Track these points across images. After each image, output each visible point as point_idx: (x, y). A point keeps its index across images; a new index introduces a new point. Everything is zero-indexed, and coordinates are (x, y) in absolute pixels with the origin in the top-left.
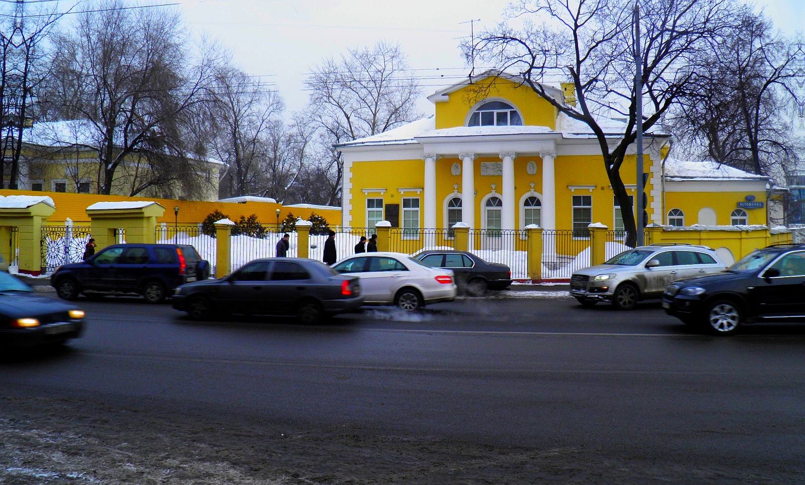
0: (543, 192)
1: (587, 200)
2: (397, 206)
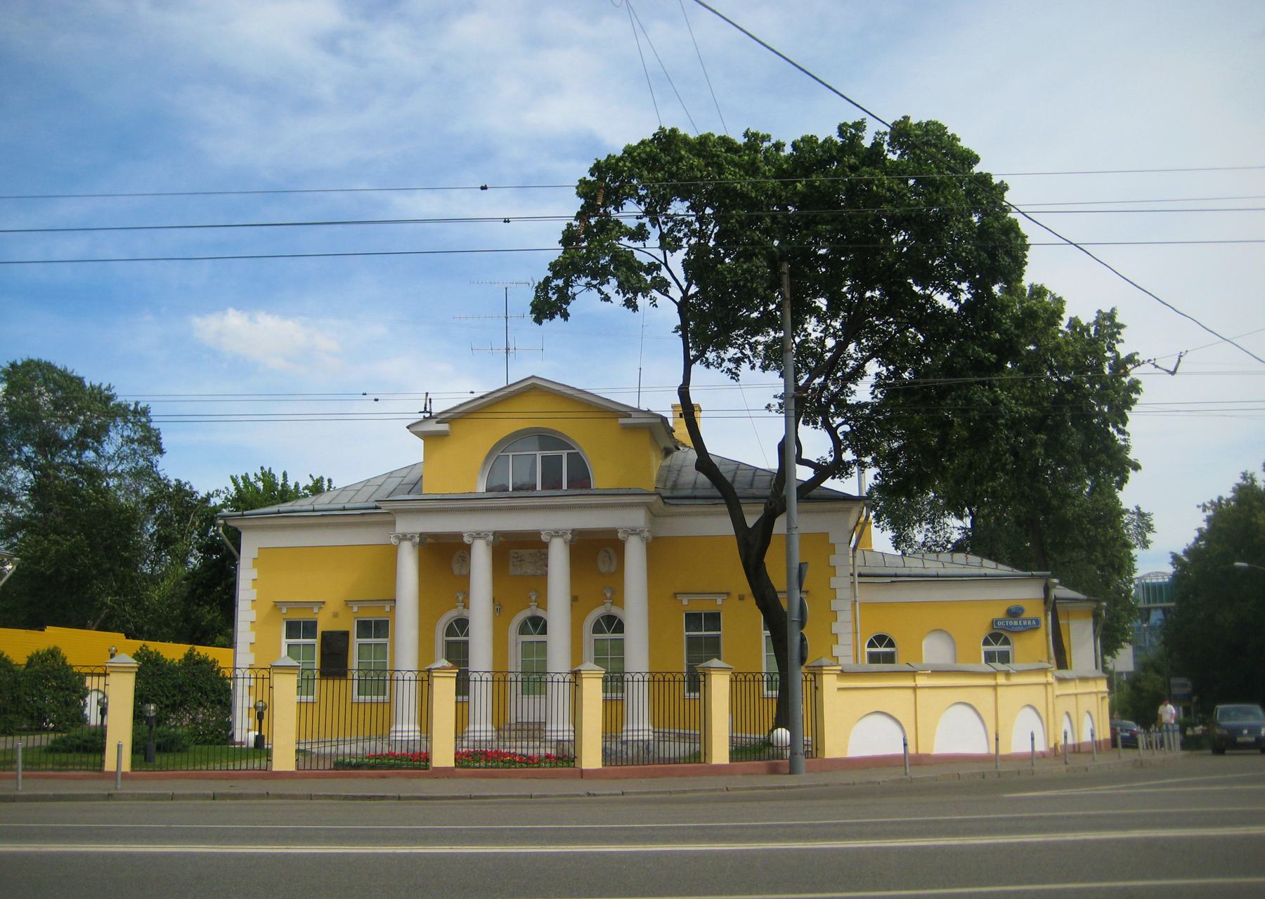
0: (548, 607)
1: (713, 620)
2: (346, 634)
